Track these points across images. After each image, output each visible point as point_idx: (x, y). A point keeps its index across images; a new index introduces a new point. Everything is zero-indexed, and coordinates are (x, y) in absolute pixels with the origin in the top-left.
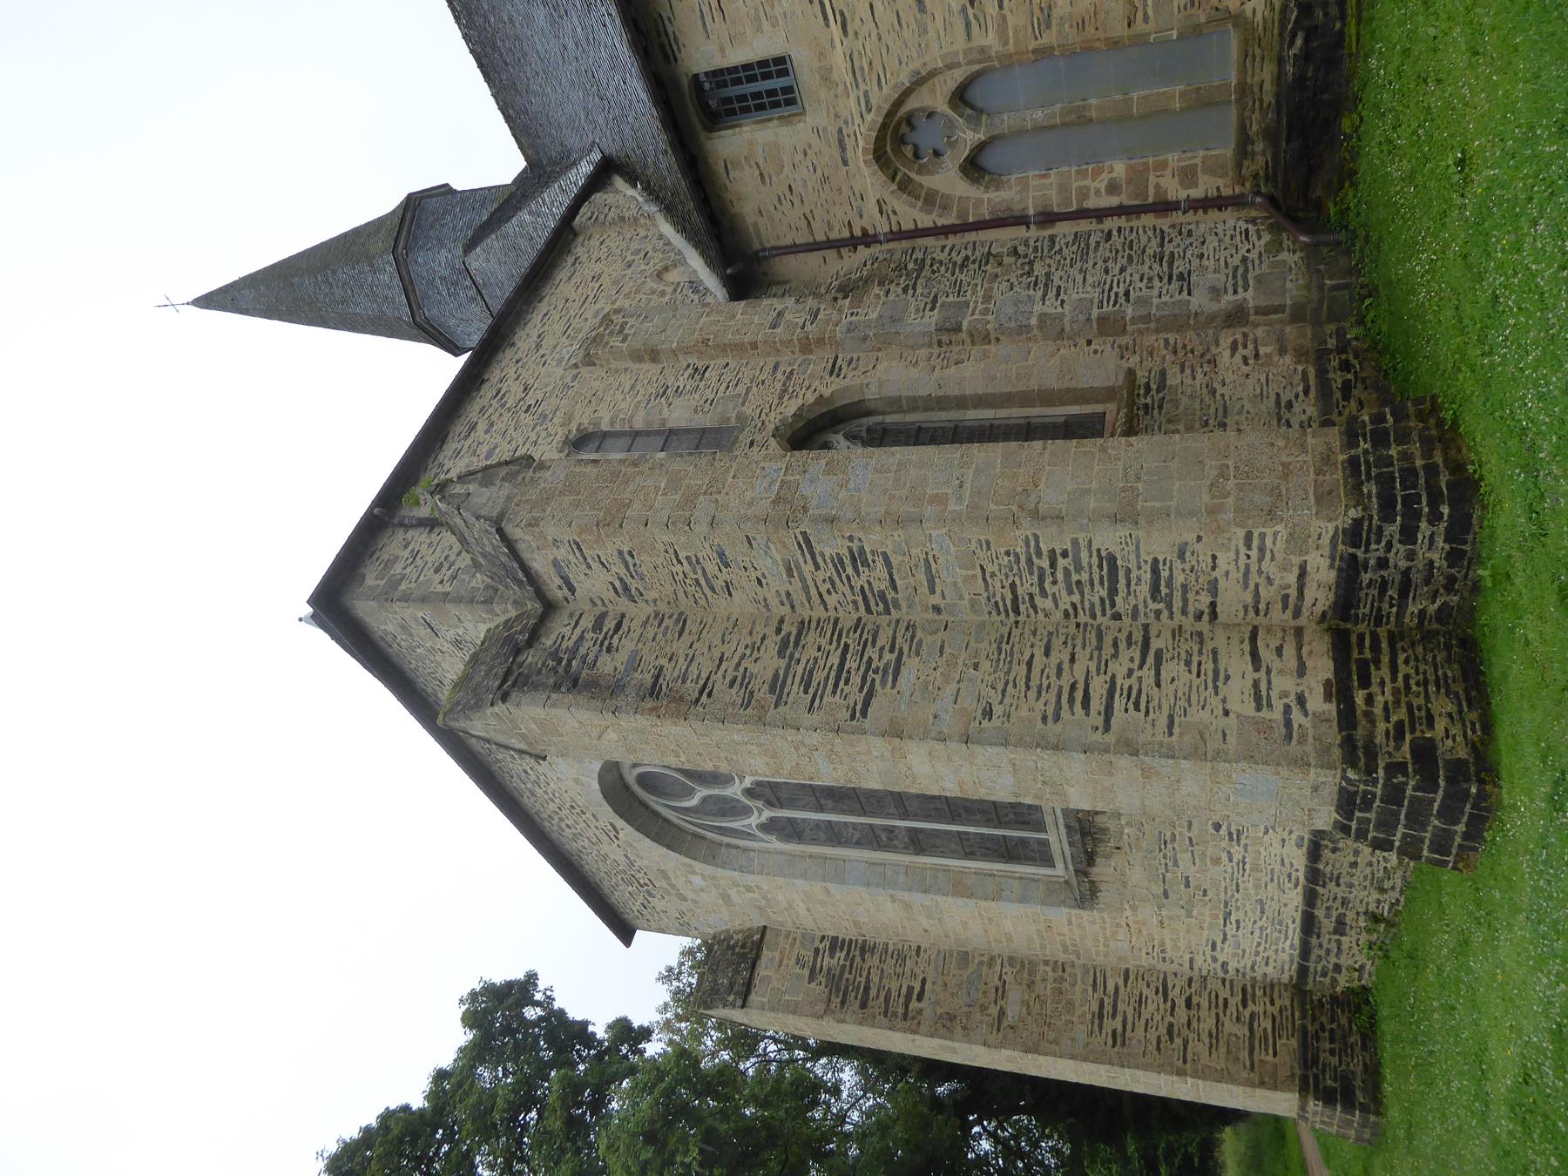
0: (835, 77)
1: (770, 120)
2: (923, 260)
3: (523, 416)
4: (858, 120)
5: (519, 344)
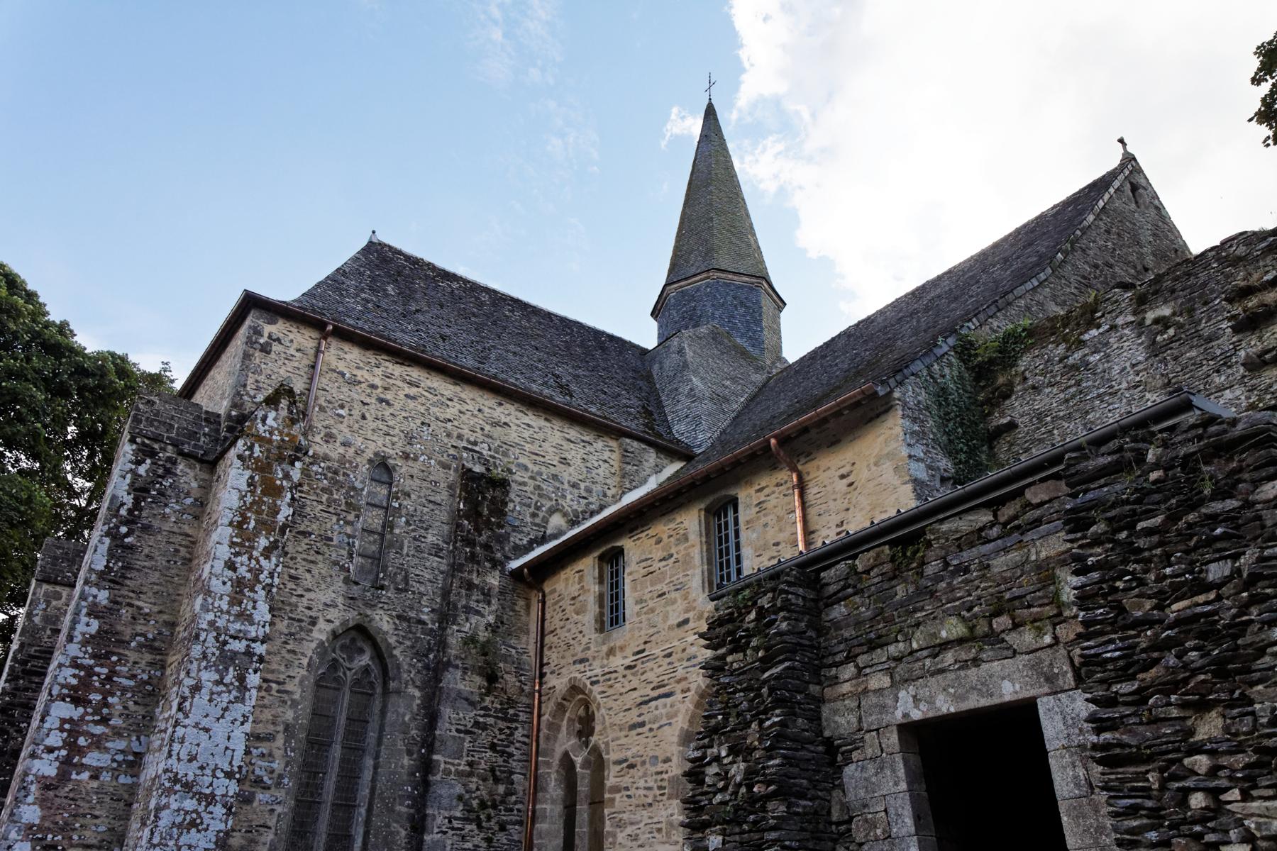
0: (611, 658)
1: (601, 606)
2: (517, 721)
3: (418, 422)
4: (589, 674)
5: (499, 409)
